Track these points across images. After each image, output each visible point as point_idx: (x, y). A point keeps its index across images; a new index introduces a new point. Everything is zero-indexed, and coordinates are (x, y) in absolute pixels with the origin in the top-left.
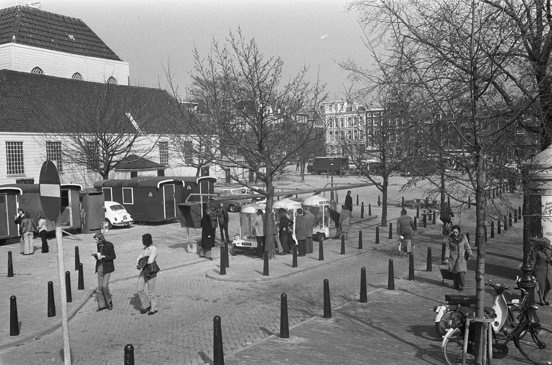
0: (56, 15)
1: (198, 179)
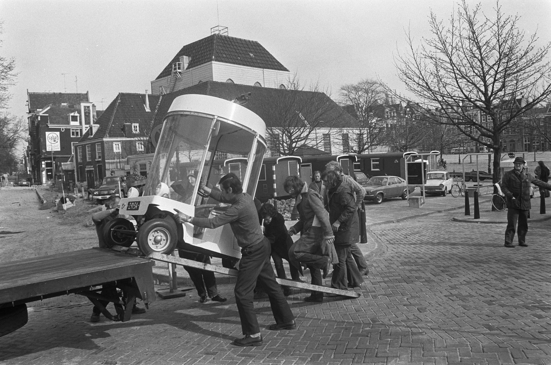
0: (240, 39)
1: (279, 159)
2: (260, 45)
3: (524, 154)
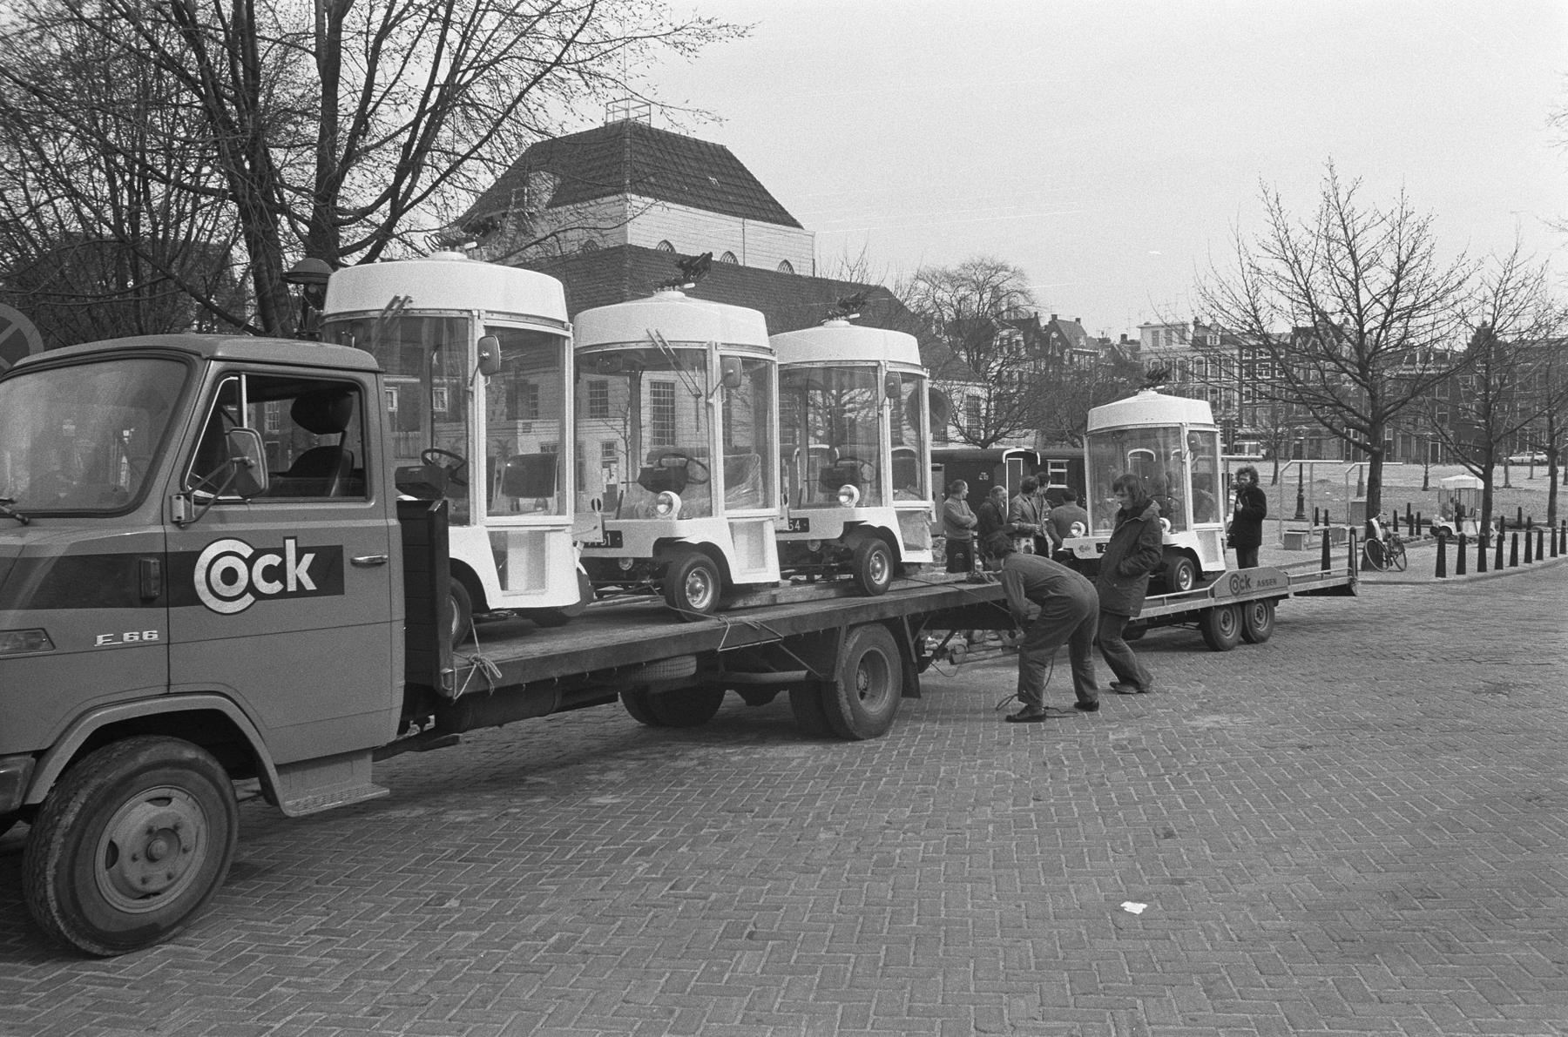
2: (731, 154)
3: (1301, 465)
